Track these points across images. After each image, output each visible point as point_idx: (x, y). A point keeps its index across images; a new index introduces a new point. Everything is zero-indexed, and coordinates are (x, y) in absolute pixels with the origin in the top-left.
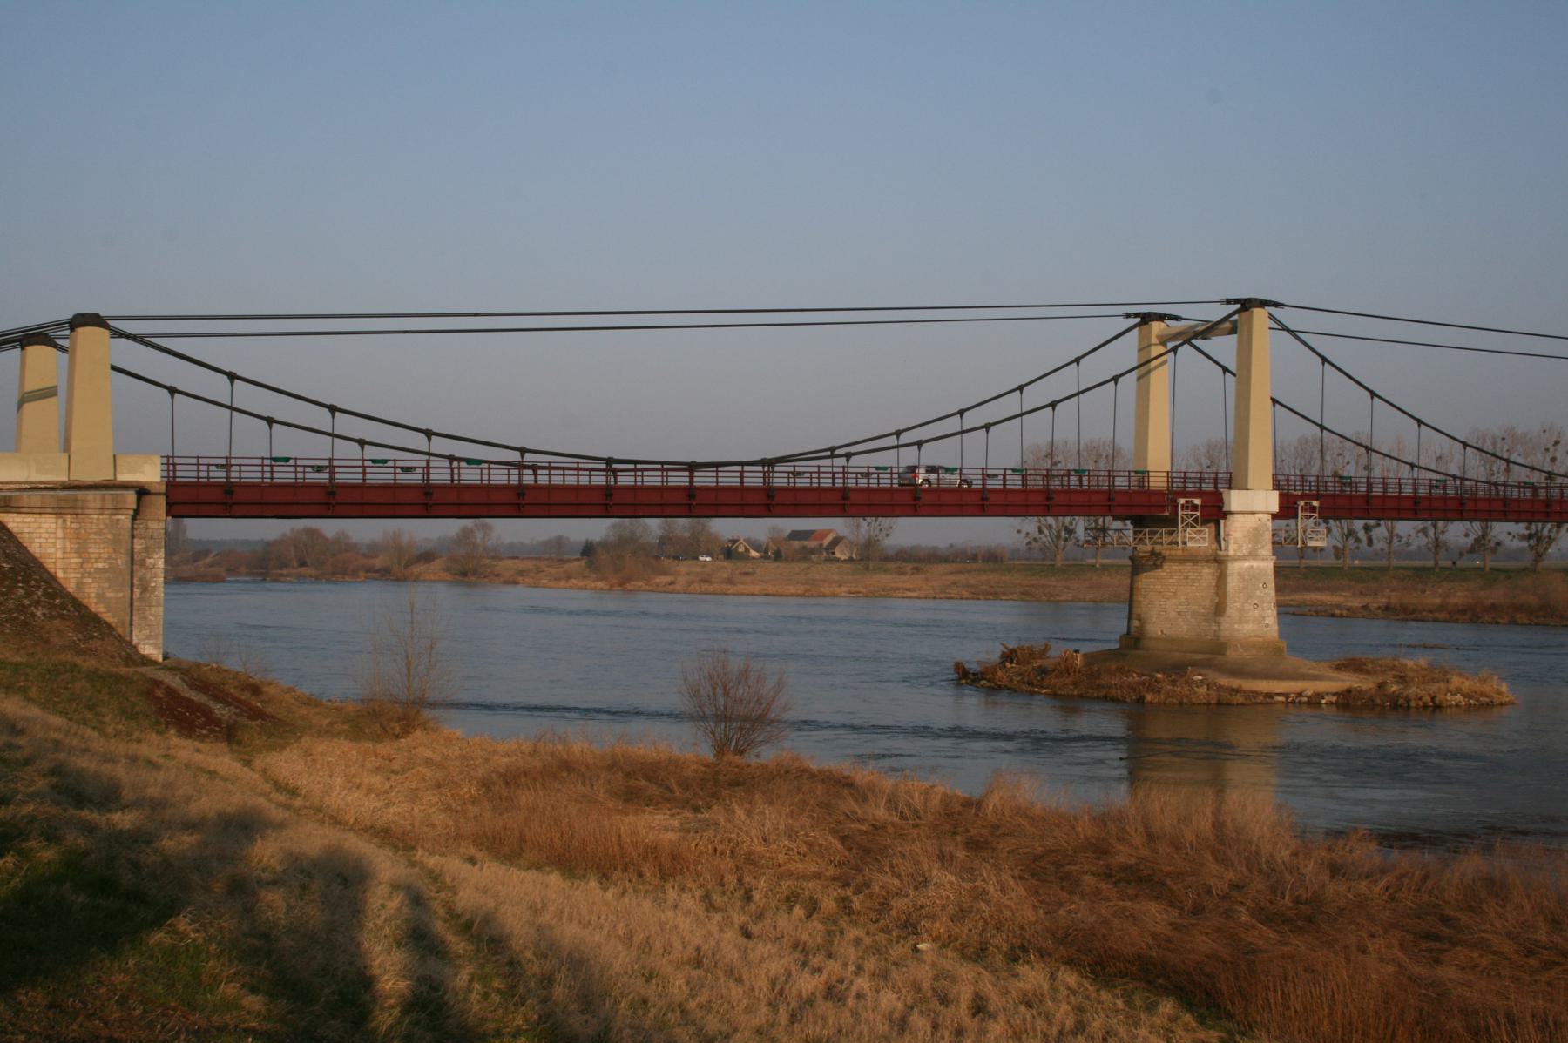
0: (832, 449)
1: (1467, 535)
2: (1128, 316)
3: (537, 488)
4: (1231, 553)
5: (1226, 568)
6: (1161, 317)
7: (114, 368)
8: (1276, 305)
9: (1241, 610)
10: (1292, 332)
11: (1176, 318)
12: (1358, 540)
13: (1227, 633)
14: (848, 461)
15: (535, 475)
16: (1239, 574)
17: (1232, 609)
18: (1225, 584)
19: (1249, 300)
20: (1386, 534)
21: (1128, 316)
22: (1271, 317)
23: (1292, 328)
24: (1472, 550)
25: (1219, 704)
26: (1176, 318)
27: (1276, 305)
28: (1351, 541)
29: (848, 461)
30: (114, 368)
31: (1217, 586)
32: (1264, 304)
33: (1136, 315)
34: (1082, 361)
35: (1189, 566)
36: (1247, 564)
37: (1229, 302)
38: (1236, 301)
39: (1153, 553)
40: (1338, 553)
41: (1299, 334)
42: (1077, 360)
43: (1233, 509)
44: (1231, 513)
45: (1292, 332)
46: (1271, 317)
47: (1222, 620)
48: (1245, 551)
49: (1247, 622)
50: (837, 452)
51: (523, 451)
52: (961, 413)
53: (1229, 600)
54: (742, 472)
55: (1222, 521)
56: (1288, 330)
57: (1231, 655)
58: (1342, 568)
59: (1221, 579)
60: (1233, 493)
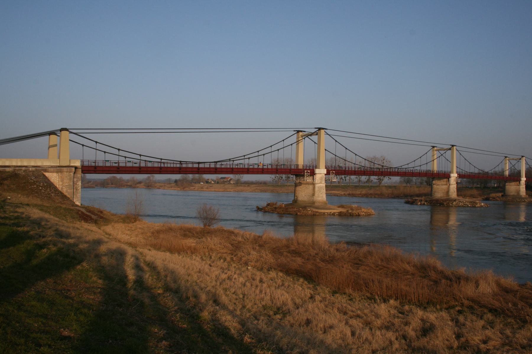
0: (230, 159)
1: (366, 179)
2: (294, 131)
3: (164, 167)
4: (316, 182)
5: (315, 186)
6: (436, 147)
7: (70, 140)
8: (326, 129)
9: (318, 195)
10: (329, 135)
11: (305, 132)
12: (343, 180)
13: (315, 200)
14: (233, 162)
15: (164, 165)
16: (318, 187)
17: (316, 195)
18: (315, 189)
19: (453, 145)
20: (349, 178)
21: (294, 131)
22: (325, 132)
23: (329, 134)
24: (366, 182)
25: (313, 215)
26: (305, 132)
27: (326, 129)
28: (342, 180)
29: (233, 162)
30: (70, 140)
31: (313, 190)
32: (323, 129)
33: (296, 131)
34: (284, 141)
35: (307, 185)
36: (320, 185)
37: (316, 128)
38: (318, 128)
39: (299, 182)
40: (339, 182)
41: (331, 136)
42: (283, 140)
43: (317, 173)
44: (316, 174)
45: (329, 135)
46: (325, 132)
47: (314, 197)
48: (319, 182)
49: (319, 197)
50: (231, 160)
51: (161, 159)
52: (258, 152)
53: (316, 193)
54: (140, 161)
55: (314, 176)
56: (328, 135)
57: (316, 204)
58: (340, 186)
59: (314, 188)
60: (317, 169)
